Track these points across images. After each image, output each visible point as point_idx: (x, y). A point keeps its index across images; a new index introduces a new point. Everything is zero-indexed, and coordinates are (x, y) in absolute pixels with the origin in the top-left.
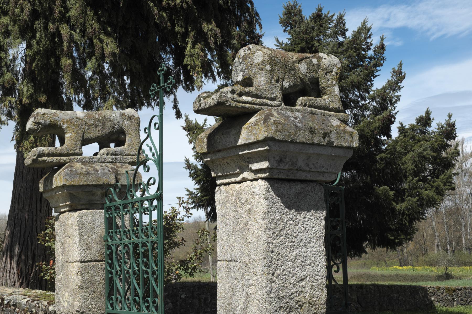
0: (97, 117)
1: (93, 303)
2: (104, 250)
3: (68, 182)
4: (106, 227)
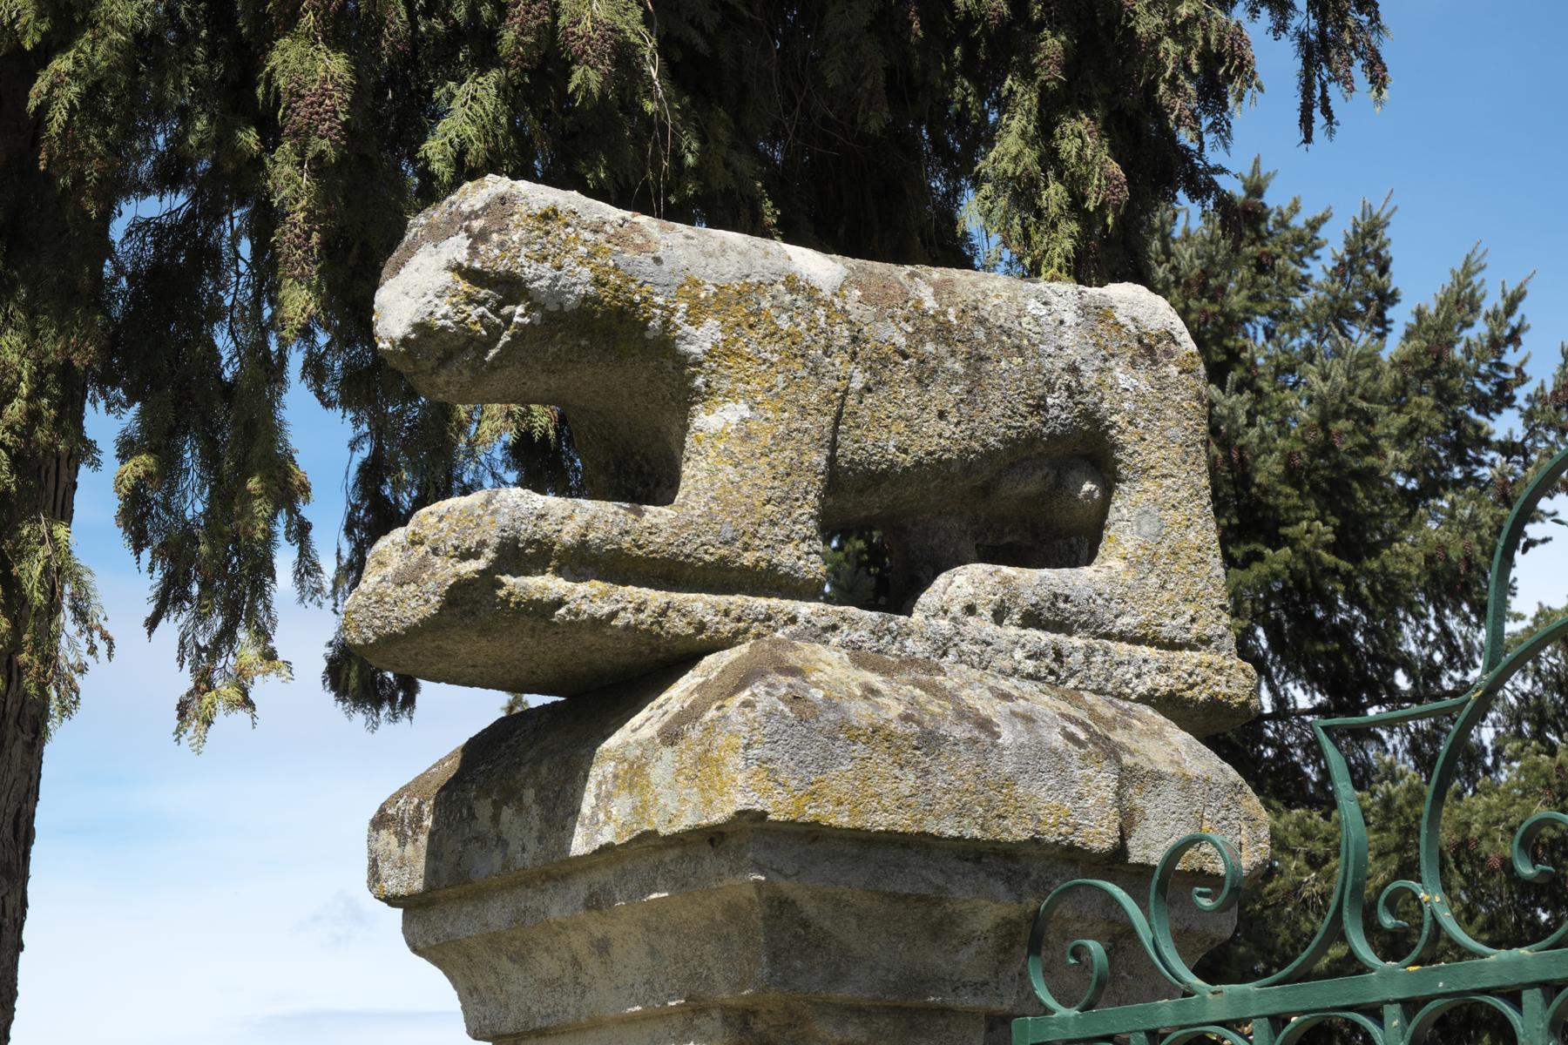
0: (930, 304)
3: (779, 795)
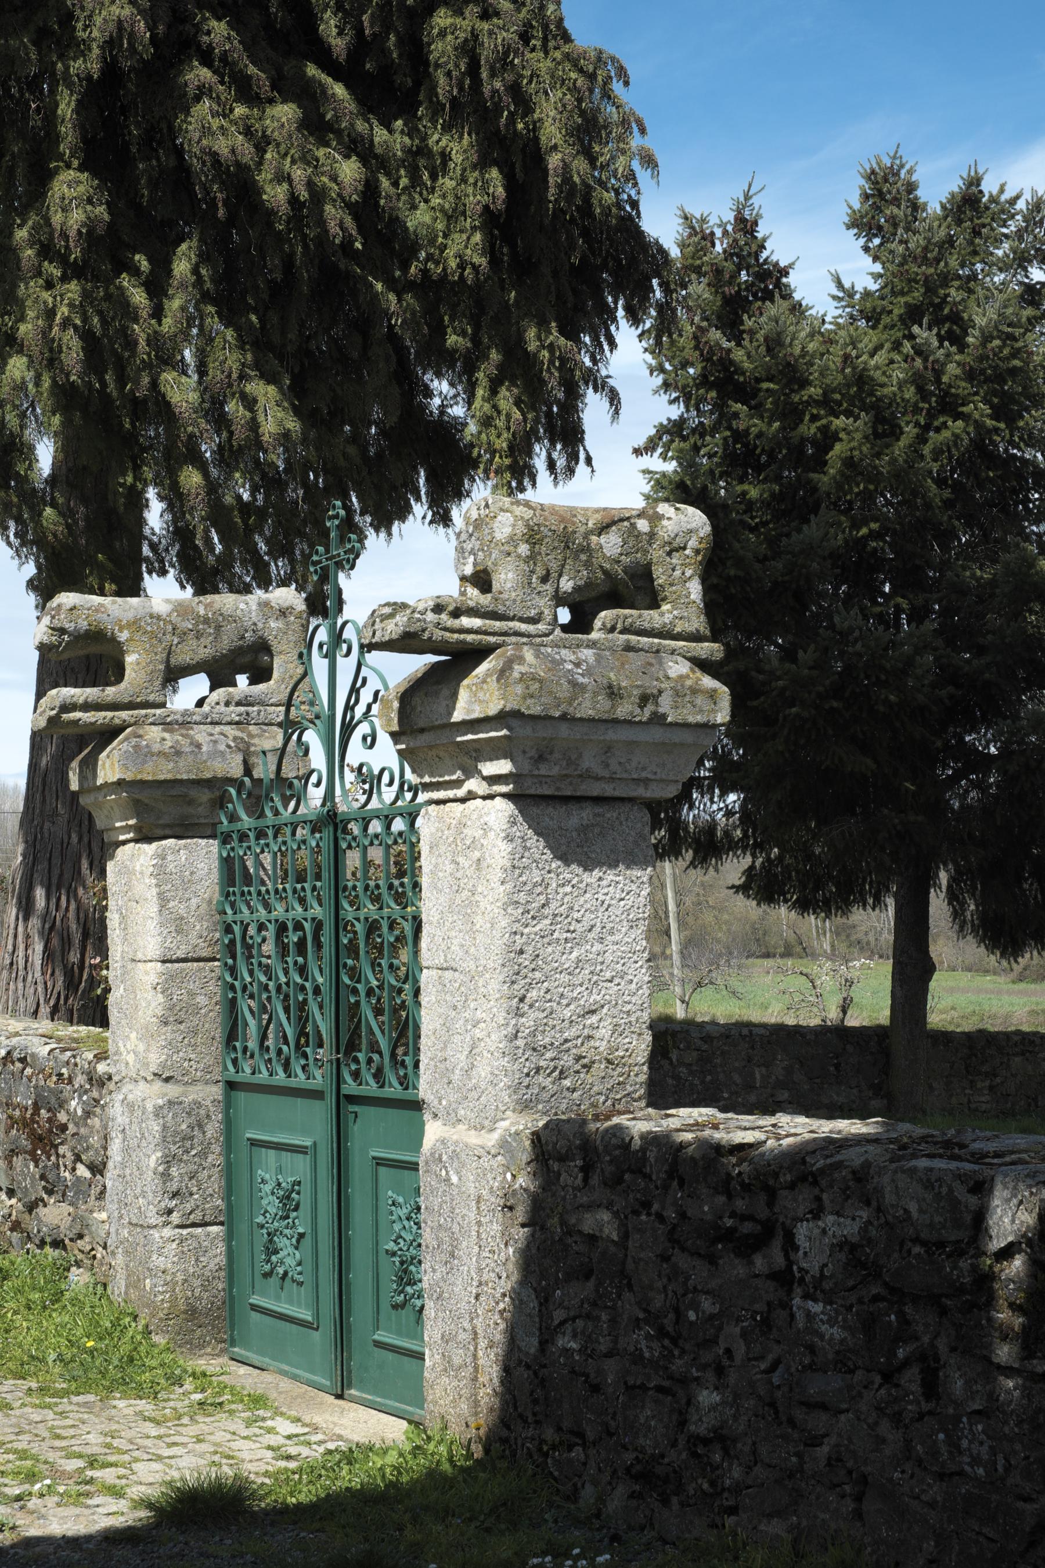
0: (202, 612)
1: (193, 1056)
2: (217, 935)
4: (221, 878)
